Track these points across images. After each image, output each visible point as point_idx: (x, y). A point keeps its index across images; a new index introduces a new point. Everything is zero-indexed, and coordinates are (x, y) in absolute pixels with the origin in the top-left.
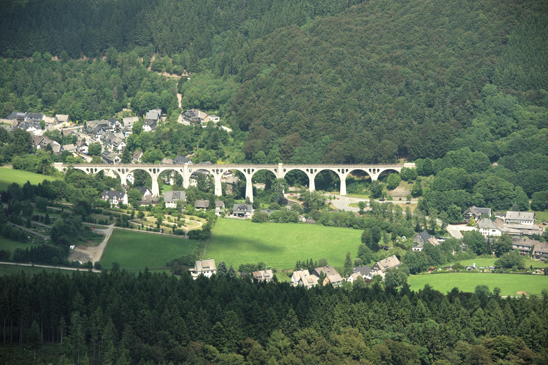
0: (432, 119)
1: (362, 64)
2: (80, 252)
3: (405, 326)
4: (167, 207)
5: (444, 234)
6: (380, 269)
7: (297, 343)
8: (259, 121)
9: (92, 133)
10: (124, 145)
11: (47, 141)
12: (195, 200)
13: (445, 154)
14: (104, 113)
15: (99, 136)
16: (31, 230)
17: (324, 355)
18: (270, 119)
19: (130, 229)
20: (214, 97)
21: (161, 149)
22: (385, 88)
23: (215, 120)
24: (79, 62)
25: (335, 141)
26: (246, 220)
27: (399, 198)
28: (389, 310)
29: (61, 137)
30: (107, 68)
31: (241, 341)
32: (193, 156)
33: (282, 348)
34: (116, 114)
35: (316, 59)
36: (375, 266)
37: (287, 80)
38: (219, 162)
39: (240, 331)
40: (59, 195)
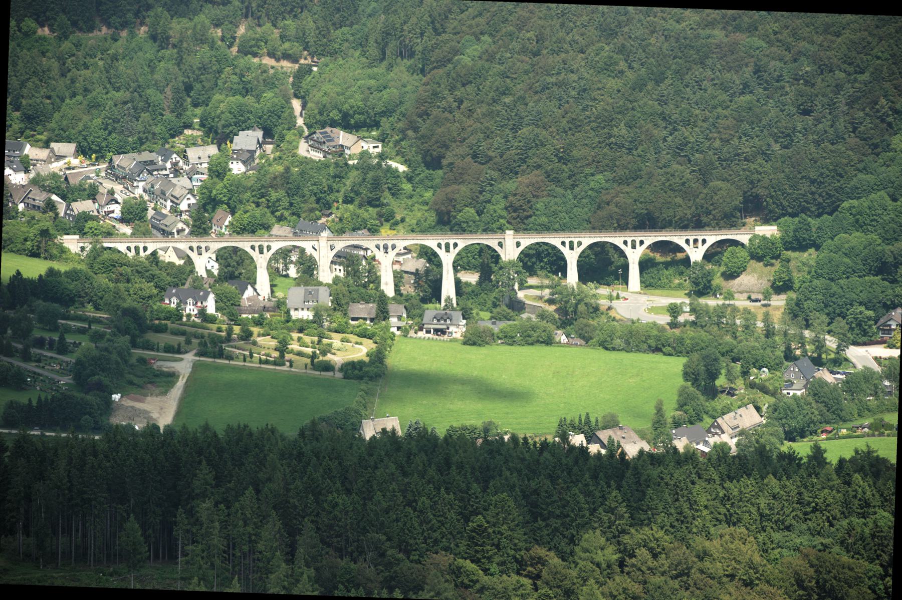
0: (811, 137)
1: (666, 33)
2: (132, 407)
3: (832, 525)
4: (294, 318)
5: (840, 364)
6: (723, 432)
7: (632, 556)
8: (463, 150)
9: (126, 178)
10: (193, 201)
11: (40, 198)
12: (348, 303)
13: (838, 206)
14: (147, 138)
15: (141, 184)
16: (31, 366)
17: (685, 578)
18: (484, 145)
19: (227, 362)
20: (369, 103)
21: (268, 207)
22: (713, 79)
23: (373, 148)
24: (93, 38)
25: (615, 185)
26: (451, 341)
27: (746, 295)
28: (800, 494)
29: (64, 186)
30: (150, 50)
31: (522, 553)
32: (333, 221)
33: (604, 566)
34: (171, 140)
35: (571, 24)
36: (713, 426)
37: (516, 67)
38: (385, 231)
39: (519, 534)
40: (80, 297)
